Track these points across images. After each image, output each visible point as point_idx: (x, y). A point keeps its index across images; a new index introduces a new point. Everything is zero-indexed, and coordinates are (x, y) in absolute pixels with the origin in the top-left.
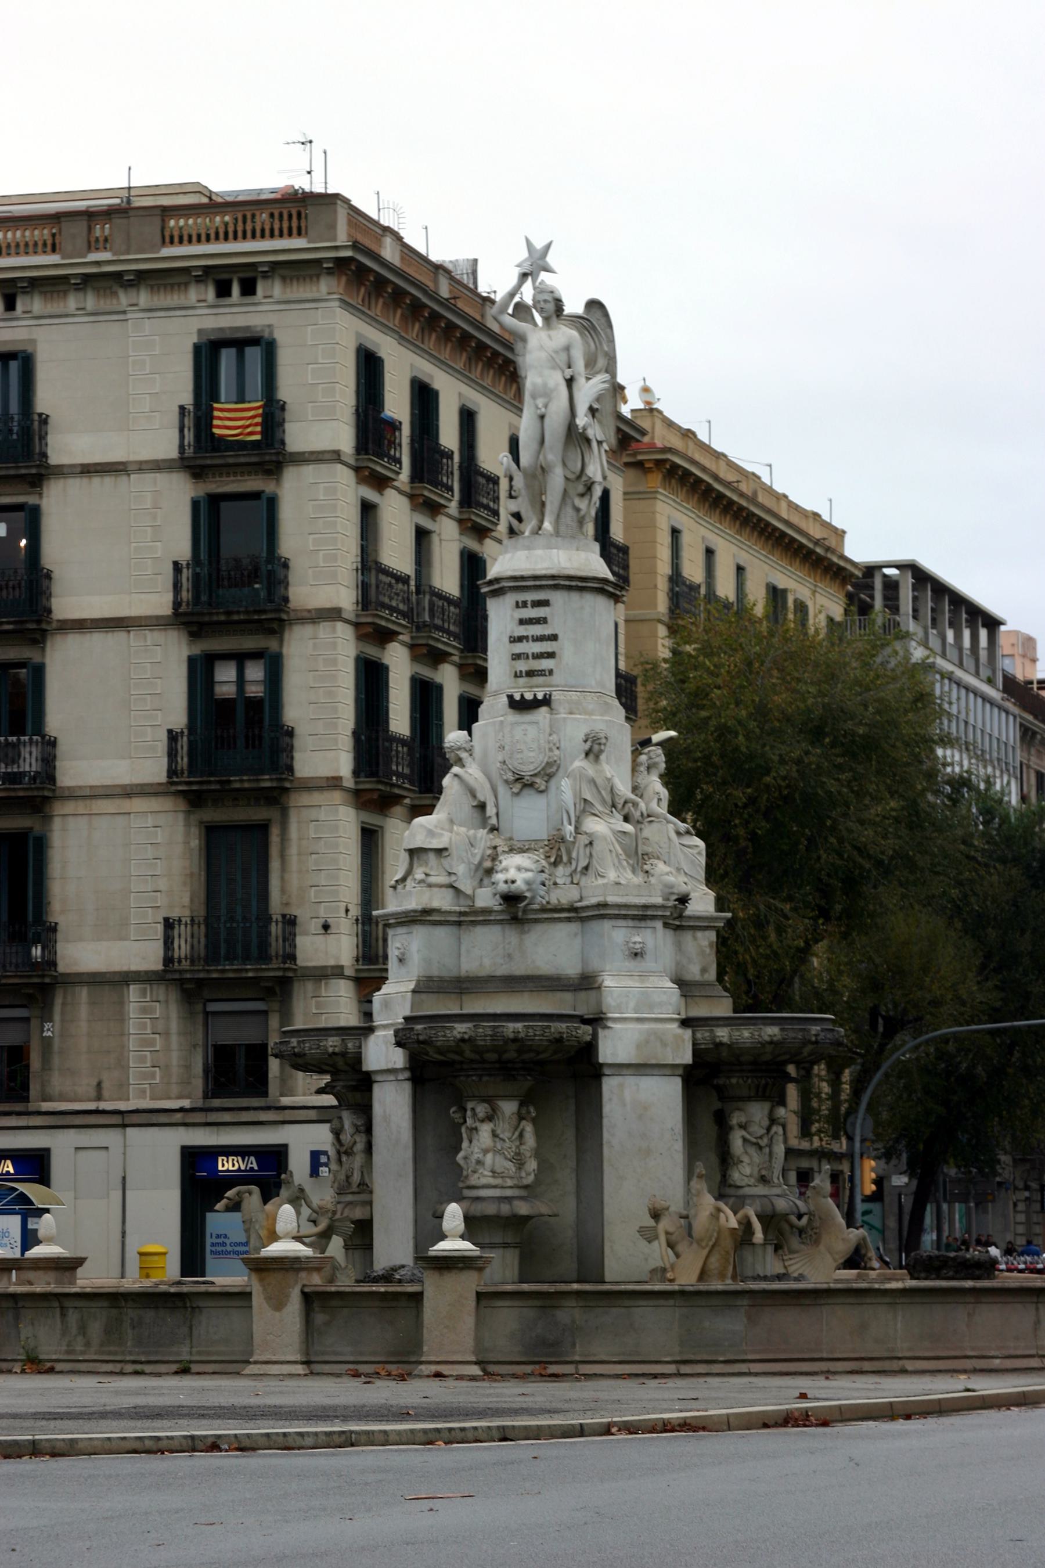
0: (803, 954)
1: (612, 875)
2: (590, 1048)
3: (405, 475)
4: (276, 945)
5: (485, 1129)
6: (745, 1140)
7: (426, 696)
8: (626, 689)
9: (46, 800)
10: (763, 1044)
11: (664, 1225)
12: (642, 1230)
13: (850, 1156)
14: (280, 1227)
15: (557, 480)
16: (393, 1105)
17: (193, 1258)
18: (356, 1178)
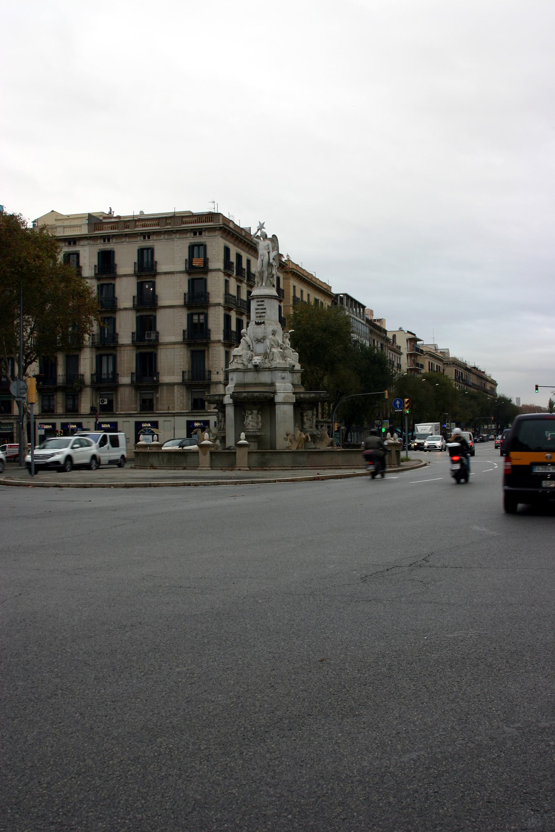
0: (322, 379)
1: (278, 361)
2: (273, 399)
3: (235, 274)
4: (207, 377)
5: (250, 417)
7: (240, 324)
8: (282, 321)
9: (157, 345)
10: (311, 398)
11: (289, 437)
12: (284, 438)
13: (332, 422)
14: (205, 438)
15: (266, 274)
16: (230, 411)
18: (222, 427)
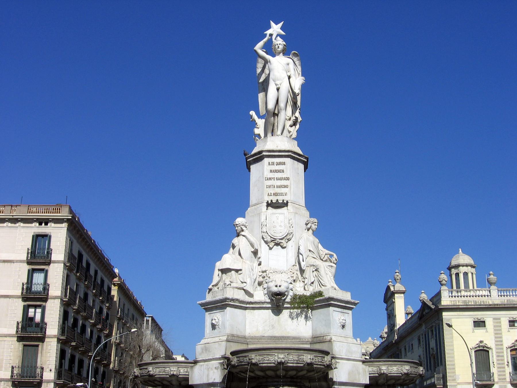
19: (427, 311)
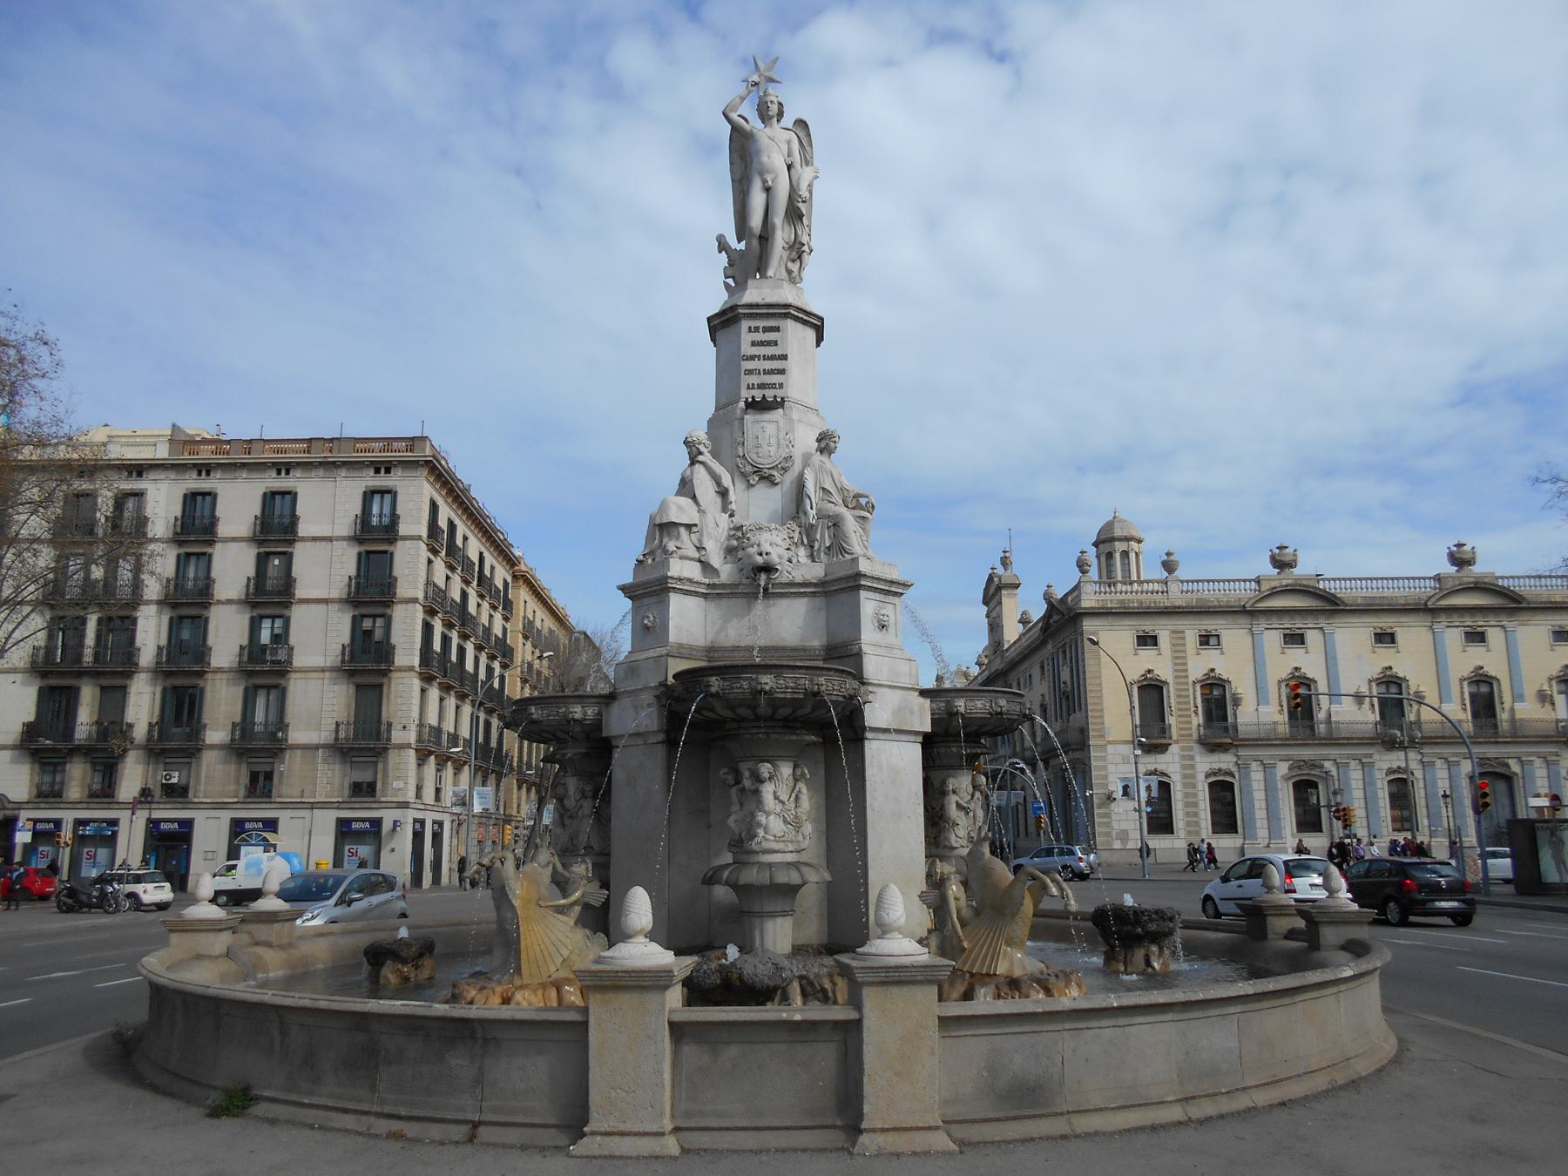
6: (958, 805)
17: (338, 861)
19: (1056, 617)
